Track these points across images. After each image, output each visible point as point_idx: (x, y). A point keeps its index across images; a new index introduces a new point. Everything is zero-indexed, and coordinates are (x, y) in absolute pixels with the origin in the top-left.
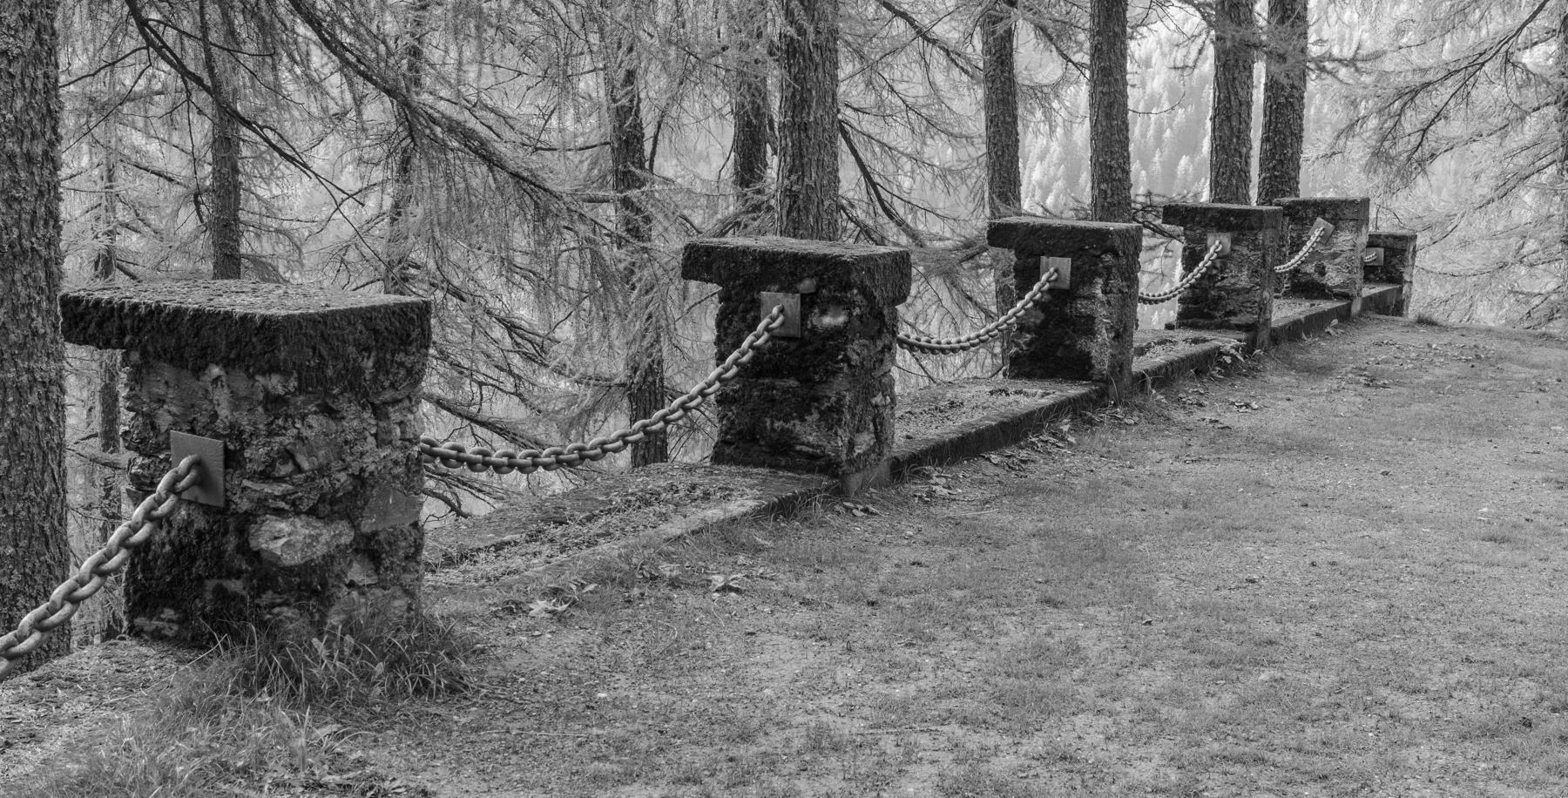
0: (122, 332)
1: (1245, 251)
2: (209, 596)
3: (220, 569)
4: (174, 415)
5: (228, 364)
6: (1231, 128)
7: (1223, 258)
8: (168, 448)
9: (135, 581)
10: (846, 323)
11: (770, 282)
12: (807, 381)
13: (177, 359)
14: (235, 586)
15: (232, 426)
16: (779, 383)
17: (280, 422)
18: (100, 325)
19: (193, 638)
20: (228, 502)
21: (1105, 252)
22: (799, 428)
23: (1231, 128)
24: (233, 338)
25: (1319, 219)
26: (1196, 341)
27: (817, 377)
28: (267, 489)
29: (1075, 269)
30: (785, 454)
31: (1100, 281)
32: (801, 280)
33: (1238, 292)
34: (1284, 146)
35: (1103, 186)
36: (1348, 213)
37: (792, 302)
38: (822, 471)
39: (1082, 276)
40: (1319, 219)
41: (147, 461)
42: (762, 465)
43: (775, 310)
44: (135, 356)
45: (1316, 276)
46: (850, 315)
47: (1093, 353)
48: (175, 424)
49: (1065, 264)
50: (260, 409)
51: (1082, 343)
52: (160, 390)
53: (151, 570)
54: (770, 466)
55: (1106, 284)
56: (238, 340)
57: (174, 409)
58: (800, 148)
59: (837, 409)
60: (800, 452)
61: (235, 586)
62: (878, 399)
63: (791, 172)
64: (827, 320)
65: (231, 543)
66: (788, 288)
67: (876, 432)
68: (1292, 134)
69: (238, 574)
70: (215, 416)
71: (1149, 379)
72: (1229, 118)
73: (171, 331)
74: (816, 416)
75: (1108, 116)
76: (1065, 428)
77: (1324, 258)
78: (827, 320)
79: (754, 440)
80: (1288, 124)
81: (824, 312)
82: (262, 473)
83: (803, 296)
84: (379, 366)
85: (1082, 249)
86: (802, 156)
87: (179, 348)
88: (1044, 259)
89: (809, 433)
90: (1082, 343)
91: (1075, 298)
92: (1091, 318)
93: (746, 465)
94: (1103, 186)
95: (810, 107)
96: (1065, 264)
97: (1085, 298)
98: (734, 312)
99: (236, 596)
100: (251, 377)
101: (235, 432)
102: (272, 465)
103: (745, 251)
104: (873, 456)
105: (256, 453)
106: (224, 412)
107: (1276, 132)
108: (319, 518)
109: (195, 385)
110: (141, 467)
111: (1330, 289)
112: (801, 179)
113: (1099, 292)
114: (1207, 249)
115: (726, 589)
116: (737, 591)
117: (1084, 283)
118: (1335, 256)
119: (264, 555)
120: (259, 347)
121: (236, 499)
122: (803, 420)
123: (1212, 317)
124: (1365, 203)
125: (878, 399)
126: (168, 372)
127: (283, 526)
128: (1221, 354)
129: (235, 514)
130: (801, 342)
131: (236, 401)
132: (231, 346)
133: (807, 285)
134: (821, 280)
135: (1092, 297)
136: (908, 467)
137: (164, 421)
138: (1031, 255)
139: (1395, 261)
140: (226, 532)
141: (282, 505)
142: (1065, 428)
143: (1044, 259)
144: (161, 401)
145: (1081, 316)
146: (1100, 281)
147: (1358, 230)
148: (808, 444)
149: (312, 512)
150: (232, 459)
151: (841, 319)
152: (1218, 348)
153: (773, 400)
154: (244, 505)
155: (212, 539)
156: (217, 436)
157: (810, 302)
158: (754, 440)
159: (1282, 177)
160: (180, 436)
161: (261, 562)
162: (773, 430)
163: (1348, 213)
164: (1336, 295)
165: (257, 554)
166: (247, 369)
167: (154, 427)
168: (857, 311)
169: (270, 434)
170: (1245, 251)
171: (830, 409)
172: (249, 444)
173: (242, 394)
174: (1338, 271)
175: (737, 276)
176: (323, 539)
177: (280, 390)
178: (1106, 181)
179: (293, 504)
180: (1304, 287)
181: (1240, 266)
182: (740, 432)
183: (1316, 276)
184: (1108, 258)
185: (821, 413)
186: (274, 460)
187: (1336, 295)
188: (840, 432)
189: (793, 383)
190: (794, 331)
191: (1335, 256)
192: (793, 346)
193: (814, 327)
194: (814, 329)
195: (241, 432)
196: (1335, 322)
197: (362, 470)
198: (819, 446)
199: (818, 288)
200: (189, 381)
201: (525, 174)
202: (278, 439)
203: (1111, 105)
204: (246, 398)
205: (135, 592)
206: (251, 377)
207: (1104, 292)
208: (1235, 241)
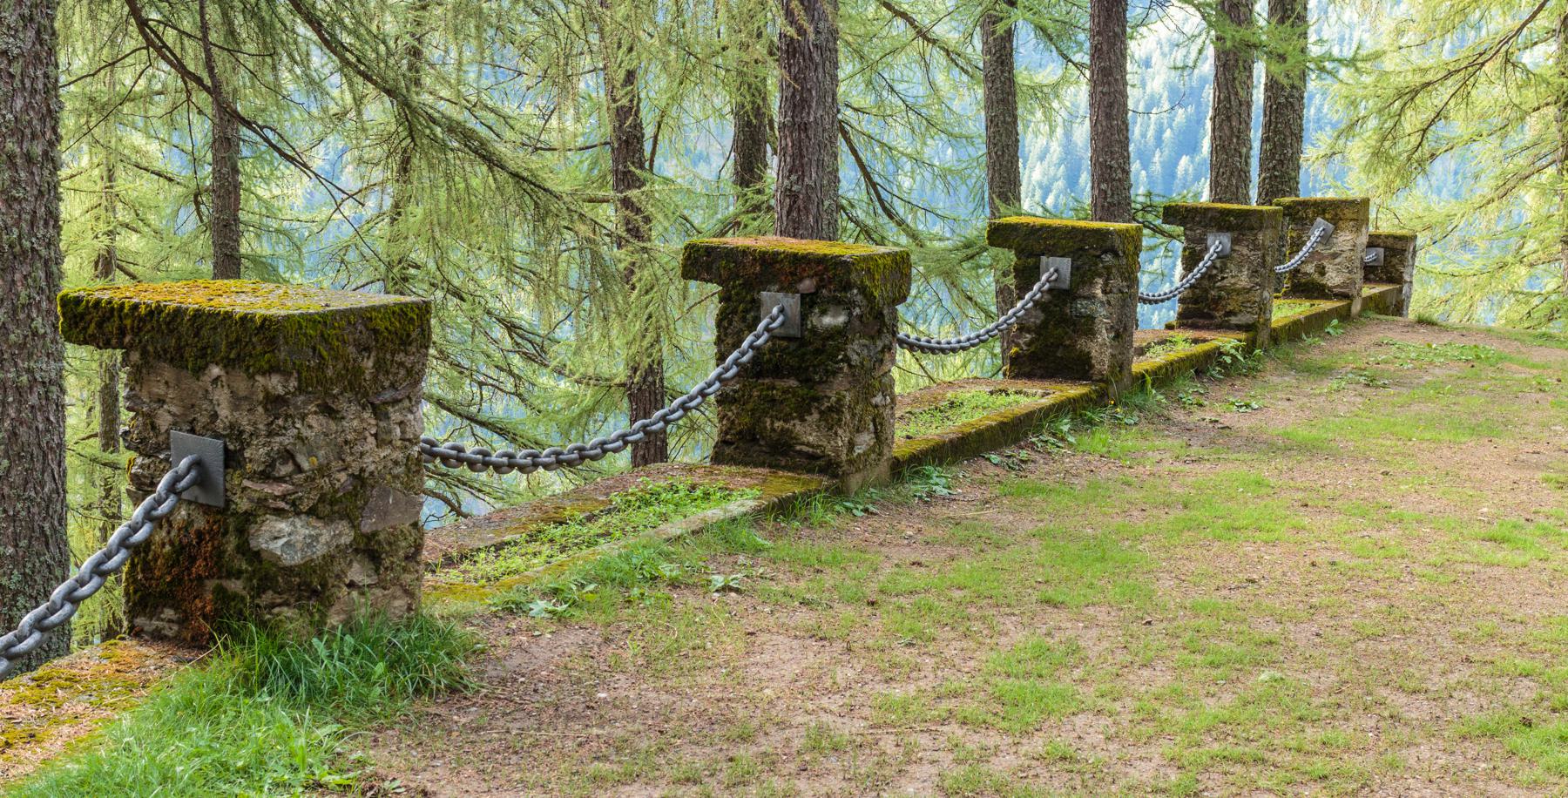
0: (122, 332)
1: (1245, 251)
2: (209, 596)
3: (220, 570)
4: (174, 415)
5: (228, 364)
6: (1231, 128)
7: (1223, 257)
8: (168, 448)
9: (135, 581)
10: (846, 324)
11: (769, 282)
12: (807, 381)
13: (177, 359)
14: (235, 586)
15: (232, 426)
16: (780, 384)
17: (280, 422)
18: (100, 325)
19: (193, 638)
20: (228, 502)
21: (1105, 252)
22: (799, 428)
23: (1231, 128)
24: (233, 337)
25: (1319, 219)
26: (1196, 341)
27: (817, 378)
28: (267, 489)
29: (1075, 269)
30: (784, 454)
31: (1100, 281)
32: (801, 280)
33: (1238, 292)
34: (1284, 146)
35: (1103, 186)
36: (1349, 213)
37: (792, 302)
38: (822, 471)
39: (1082, 276)
40: (1319, 219)
41: (147, 461)
42: (762, 465)
43: (775, 310)
44: (135, 357)
45: (1316, 276)
46: (850, 314)
47: (1093, 354)
48: (175, 424)
49: (1065, 264)
50: (260, 409)
51: (1082, 343)
52: (160, 390)
53: (151, 570)
54: (770, 466)
55: (1106, 284)
56: (238, 340)
57: (174, 409)
58: (800, 149)
59: (837, 409)
60: (800, 452)
61: (235, 586)
62: (878, 399)
63: (791, 172)
64: (827, 320)
65: (231, 543)
66: (788, 288)
67: (876, 432)
68: (1292, 133)
69: (238, 574)
70: (215, 416)
71: (1149, 379)
72: (1229, 118)
73: (171, 331)
74: (816, 416)
75: (1108, 116)
76: (1065, 428)
77: (1324, 258)
78: (827, 320)
79: (754, 440)
80: (1287, 124)
81: (824, 313)
82: (262, 473)
83: (803, 296)
84: (379, 366)
85: (1082, 249)
86: (802, 157)
87: (179, 349)
88: (1044, 259)
89: (808, 433)
90: (1082, 343)
91: (1075, 299)
92: (1091, 318)
93: (746, 465)
94: (1103, 186)
95: (810, 107)
96: (1065, 264)
97: (1085, 298)
98: (734, 312)
99: (235, 596)
100: (251, 377)
101: (235, 431)
102: (272, 465)
103: (745, 252)
104: (873, 456)
105: (256, 453)
106: (224, 412)
107: (1275, 132)
108: (319, 518)
109: (195, 385)
110: (141, 467)
111: (1330, 289)
112: (801, 179)
113: (1099, 292)
114: (1207, 249)
115: (726, 589)
116: (737, 591)
117: (1084, 283)
118: (1335, 256)
119: (264, 556)
120: (259, 348)
121: (236, 499)
122: (803, 420)
123: (1212, 317)
124: (1365, 203)
125: (878, 399)
126: (168, 373)
127: (283, 526)
128: (1221, 354)
129: (235, 514)
130: (801, 341)
131: (236, 401)
132: (231, 346)
133: (807, 285)
134: (822, 280)
135: (1092, 297)
136: (906, 468)
137: (164, 421)
138: (1031, 255)
139: (1395, 261)
140: (226, 533)
141: (282, 505)
142: (1065, 428)
143: (1044, 259)
144: (161, 401)
145: (1081, 316)
146: (1100, 281)
147: (1358, 230)
148: (808, 444)
149: (312, 512)
150: (232, 459)
151: (841, 319)
152: (1218, 348)
153: (773, 400)
154: (243, 505)
155: (212, 539)
156: (217, 436)
157: (810, 302)
158: (754, 440)
159: (1282, 177)
160: (180, 436)
161: (261, 562)
162: (773, 430)
163: (1349, 213)
164: (1336, 295)
165: (257, 555)
166: (247, 369)
167: (154, 427)
168: (857, 311)
169: (270, 434)
170: (1245, 251)
171: (830, 409)
172: (249, 445)
173: (242, 393)
174: (1338, 271)
175: (738, 276)
176: (323, 539)
177: (280, 390)
178: (1106, 181)
179: (293, 504)
180: (1304, 288)
181: (1240, 266)
182: (740, 432)
183: (1316, 276)
184: (1108, 258)
185: (821, 413)
186: (274, 460)
187: (1336, 295)
188: (840, 432)
189: (793, 383)
190: (794, 331)
191: (1335, 256)
192: (793, 346)
193: (814, 327)
194: (814, 330)
195: (241, 433)
196: (1335, 322)
197: (362, 470)
198: (819, 446)
199: (818, 288)
200: (189, 382)
201: (525, 174)
202: (278, 439)
203: (1111, 105)
204: (246, 398)
205: (135, 592)
206: (251, 377)
207: (1104, 292)
208: (1235, 241)
